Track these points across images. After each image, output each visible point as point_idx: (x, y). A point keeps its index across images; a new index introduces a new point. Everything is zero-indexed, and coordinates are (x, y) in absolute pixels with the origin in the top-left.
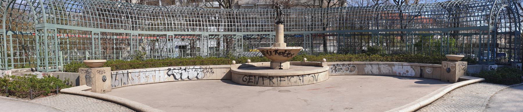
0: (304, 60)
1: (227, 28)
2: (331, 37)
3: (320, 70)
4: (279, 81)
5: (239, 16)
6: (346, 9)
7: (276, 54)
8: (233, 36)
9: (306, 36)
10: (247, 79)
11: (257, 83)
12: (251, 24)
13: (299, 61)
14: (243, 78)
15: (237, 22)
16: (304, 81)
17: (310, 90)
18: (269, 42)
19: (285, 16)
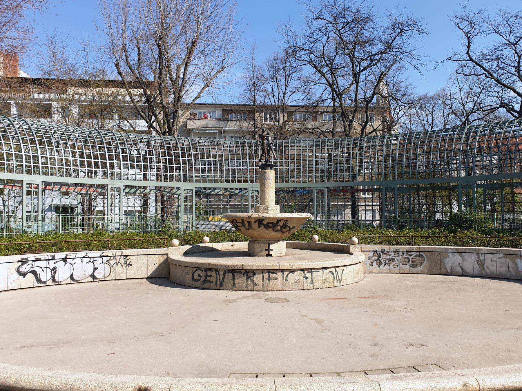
0: (313, 238)
1: (162, 173)
2: (366, 193)
3: (348, 260)
4: (266, 281)
5: (187, 151)
6: (399, 138)
7: (259, 227)
8: (174, 191)
9: (317, 191)
10: (201, 277)
11: (221, 285)
12: (212, 167)
13: (303, 241)
14: (193, 274)
15: (184, 163)
16: (314, 282)
17: (326, 299)
18: (246, 202)
19: (278, 154)
